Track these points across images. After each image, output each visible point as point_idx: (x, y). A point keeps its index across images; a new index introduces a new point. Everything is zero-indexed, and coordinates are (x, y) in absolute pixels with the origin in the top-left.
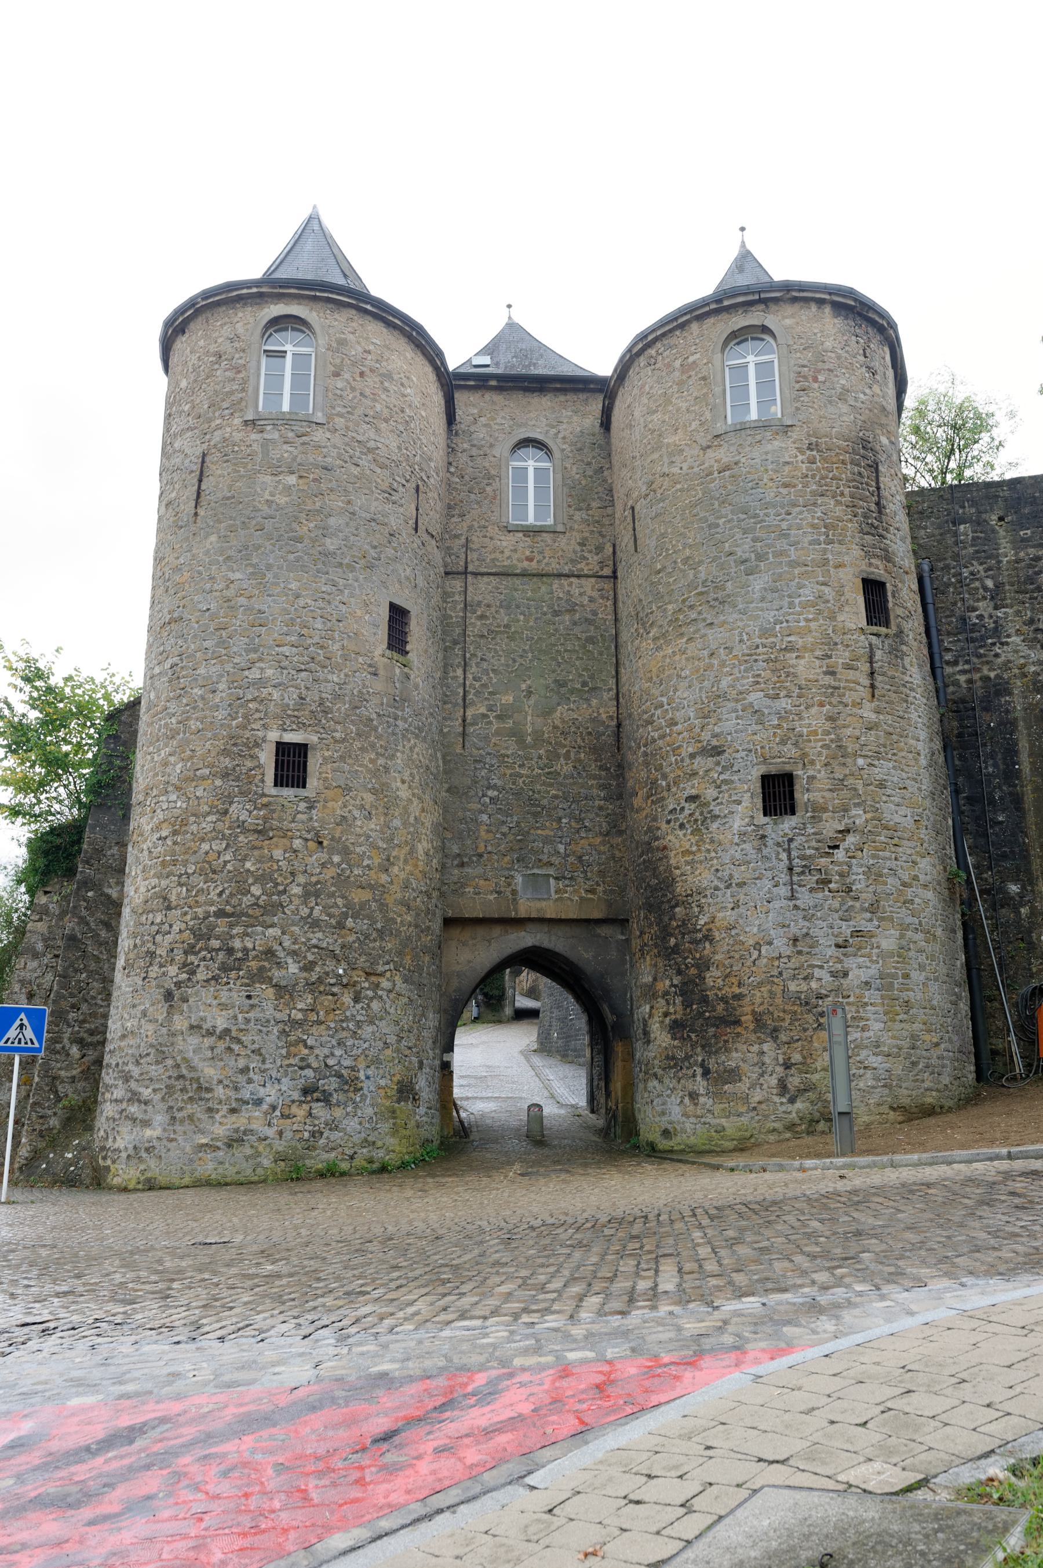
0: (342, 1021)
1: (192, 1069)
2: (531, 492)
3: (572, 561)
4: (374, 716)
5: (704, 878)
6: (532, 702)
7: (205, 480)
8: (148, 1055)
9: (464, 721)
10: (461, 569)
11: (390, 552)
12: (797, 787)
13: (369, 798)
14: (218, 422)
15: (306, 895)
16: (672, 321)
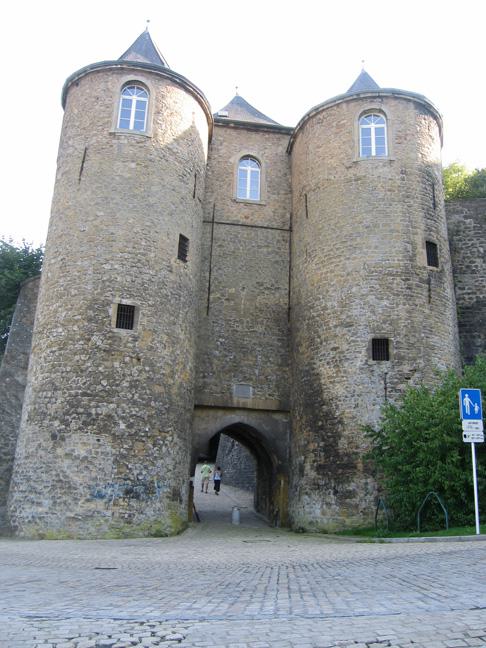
1: (66, 477)
2: (249, 184)
10: (211, 220)
11: (181, 207)
13: (165, 338)
15: (131, 387)
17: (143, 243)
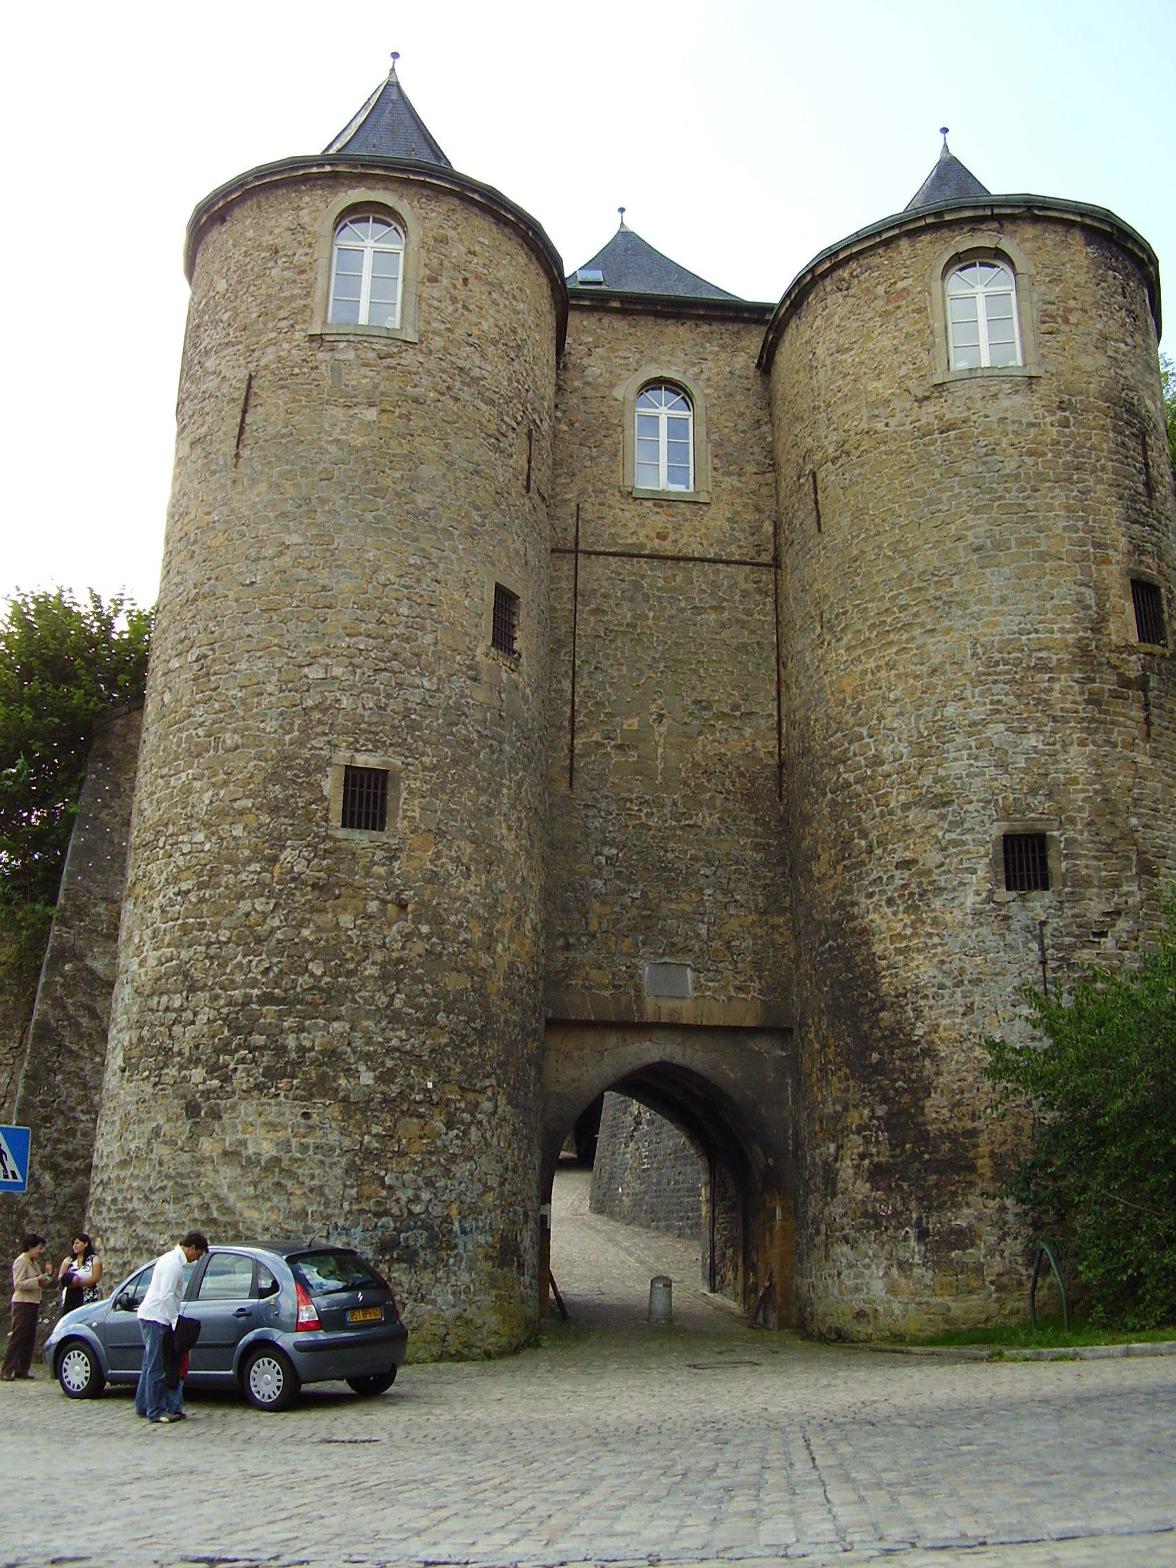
0: (431, 1153)
1: (229, 1210)
2: (662, 451)
3: (719, 542)
4: (475, 736)
5: (923, 970)
6: (663, 729)
7: (251, 411)
8: (163, 1188)
9: (572, 751)
12: (1052, 852)
13: (468, 848)
14: (273, 335)
15: (384, 977)
16: (874, 235)
17: (404, 610)
